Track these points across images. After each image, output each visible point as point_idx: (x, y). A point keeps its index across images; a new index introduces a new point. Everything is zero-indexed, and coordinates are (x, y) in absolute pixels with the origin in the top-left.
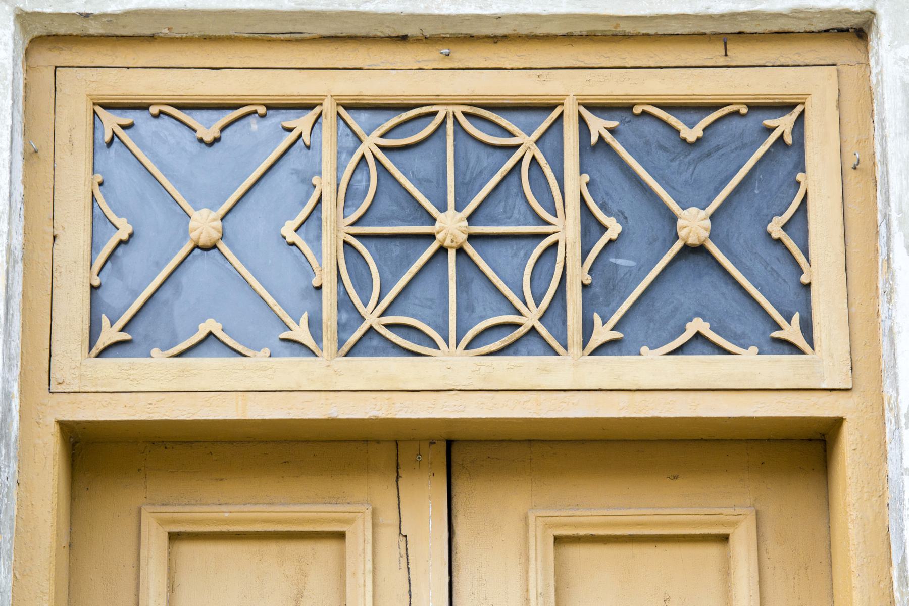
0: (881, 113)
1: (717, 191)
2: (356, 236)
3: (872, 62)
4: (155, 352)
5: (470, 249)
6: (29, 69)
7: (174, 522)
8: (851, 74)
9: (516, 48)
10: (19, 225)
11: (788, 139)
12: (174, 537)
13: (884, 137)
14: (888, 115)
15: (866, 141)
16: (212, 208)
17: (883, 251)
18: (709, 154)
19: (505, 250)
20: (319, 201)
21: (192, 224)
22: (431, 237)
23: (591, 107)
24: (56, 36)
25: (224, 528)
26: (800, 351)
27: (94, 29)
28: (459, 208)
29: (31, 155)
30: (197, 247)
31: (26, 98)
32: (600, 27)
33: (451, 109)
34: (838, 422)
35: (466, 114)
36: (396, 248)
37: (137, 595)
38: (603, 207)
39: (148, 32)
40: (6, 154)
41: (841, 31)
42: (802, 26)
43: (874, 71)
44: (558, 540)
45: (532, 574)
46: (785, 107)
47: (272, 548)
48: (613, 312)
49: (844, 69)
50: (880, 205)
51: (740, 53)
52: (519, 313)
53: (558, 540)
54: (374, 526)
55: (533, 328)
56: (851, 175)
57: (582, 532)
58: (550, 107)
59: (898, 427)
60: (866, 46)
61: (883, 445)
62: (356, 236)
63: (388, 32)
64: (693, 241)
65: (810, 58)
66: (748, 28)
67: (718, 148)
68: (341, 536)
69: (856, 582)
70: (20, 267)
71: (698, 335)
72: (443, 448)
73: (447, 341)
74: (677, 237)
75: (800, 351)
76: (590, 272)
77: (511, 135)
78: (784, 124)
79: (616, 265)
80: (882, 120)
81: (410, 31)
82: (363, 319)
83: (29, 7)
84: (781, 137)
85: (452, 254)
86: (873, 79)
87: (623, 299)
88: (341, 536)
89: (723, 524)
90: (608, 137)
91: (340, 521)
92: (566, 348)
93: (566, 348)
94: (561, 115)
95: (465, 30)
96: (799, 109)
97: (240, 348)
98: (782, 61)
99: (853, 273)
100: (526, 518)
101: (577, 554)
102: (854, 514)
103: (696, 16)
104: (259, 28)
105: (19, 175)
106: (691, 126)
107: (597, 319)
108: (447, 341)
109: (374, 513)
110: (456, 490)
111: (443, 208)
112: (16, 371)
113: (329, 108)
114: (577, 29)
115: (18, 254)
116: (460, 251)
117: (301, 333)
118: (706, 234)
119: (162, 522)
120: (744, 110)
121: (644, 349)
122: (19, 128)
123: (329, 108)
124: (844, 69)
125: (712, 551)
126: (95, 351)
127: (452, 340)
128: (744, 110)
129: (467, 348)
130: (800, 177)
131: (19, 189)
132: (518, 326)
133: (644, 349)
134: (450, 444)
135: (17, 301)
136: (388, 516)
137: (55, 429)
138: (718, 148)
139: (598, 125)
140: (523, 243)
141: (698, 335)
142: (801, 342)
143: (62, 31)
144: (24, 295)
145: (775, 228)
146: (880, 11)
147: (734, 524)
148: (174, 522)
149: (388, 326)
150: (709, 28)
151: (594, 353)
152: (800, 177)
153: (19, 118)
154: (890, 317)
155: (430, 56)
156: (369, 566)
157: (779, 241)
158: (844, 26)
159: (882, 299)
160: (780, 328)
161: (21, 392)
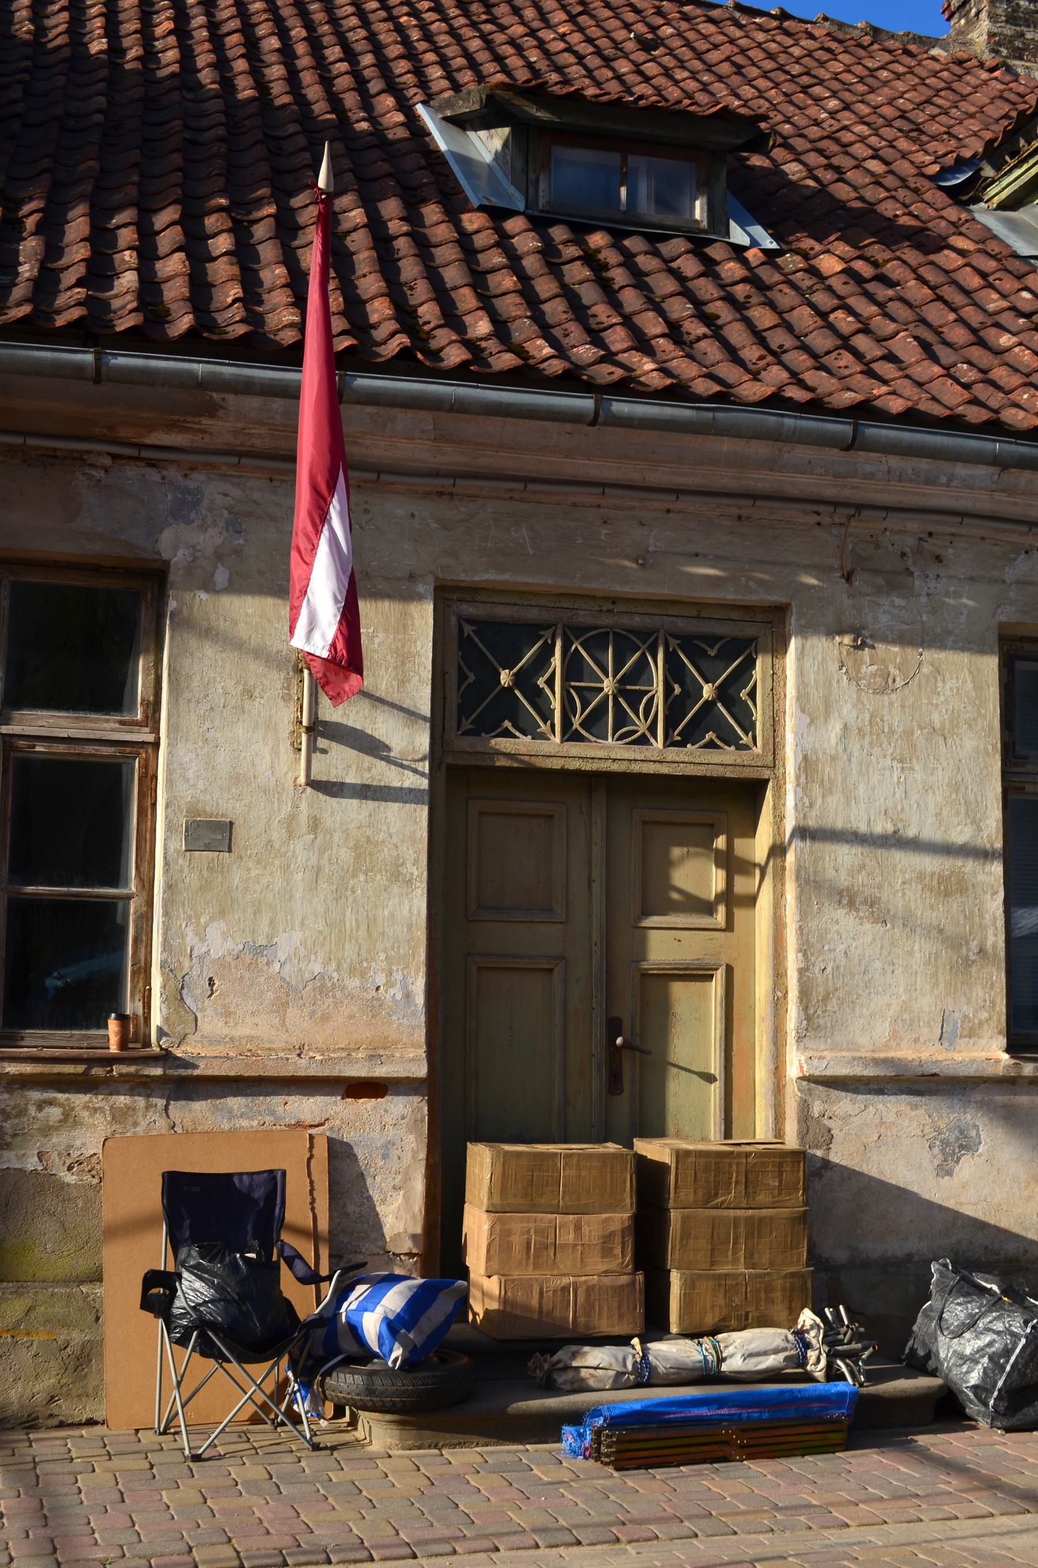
58: (651, 634)
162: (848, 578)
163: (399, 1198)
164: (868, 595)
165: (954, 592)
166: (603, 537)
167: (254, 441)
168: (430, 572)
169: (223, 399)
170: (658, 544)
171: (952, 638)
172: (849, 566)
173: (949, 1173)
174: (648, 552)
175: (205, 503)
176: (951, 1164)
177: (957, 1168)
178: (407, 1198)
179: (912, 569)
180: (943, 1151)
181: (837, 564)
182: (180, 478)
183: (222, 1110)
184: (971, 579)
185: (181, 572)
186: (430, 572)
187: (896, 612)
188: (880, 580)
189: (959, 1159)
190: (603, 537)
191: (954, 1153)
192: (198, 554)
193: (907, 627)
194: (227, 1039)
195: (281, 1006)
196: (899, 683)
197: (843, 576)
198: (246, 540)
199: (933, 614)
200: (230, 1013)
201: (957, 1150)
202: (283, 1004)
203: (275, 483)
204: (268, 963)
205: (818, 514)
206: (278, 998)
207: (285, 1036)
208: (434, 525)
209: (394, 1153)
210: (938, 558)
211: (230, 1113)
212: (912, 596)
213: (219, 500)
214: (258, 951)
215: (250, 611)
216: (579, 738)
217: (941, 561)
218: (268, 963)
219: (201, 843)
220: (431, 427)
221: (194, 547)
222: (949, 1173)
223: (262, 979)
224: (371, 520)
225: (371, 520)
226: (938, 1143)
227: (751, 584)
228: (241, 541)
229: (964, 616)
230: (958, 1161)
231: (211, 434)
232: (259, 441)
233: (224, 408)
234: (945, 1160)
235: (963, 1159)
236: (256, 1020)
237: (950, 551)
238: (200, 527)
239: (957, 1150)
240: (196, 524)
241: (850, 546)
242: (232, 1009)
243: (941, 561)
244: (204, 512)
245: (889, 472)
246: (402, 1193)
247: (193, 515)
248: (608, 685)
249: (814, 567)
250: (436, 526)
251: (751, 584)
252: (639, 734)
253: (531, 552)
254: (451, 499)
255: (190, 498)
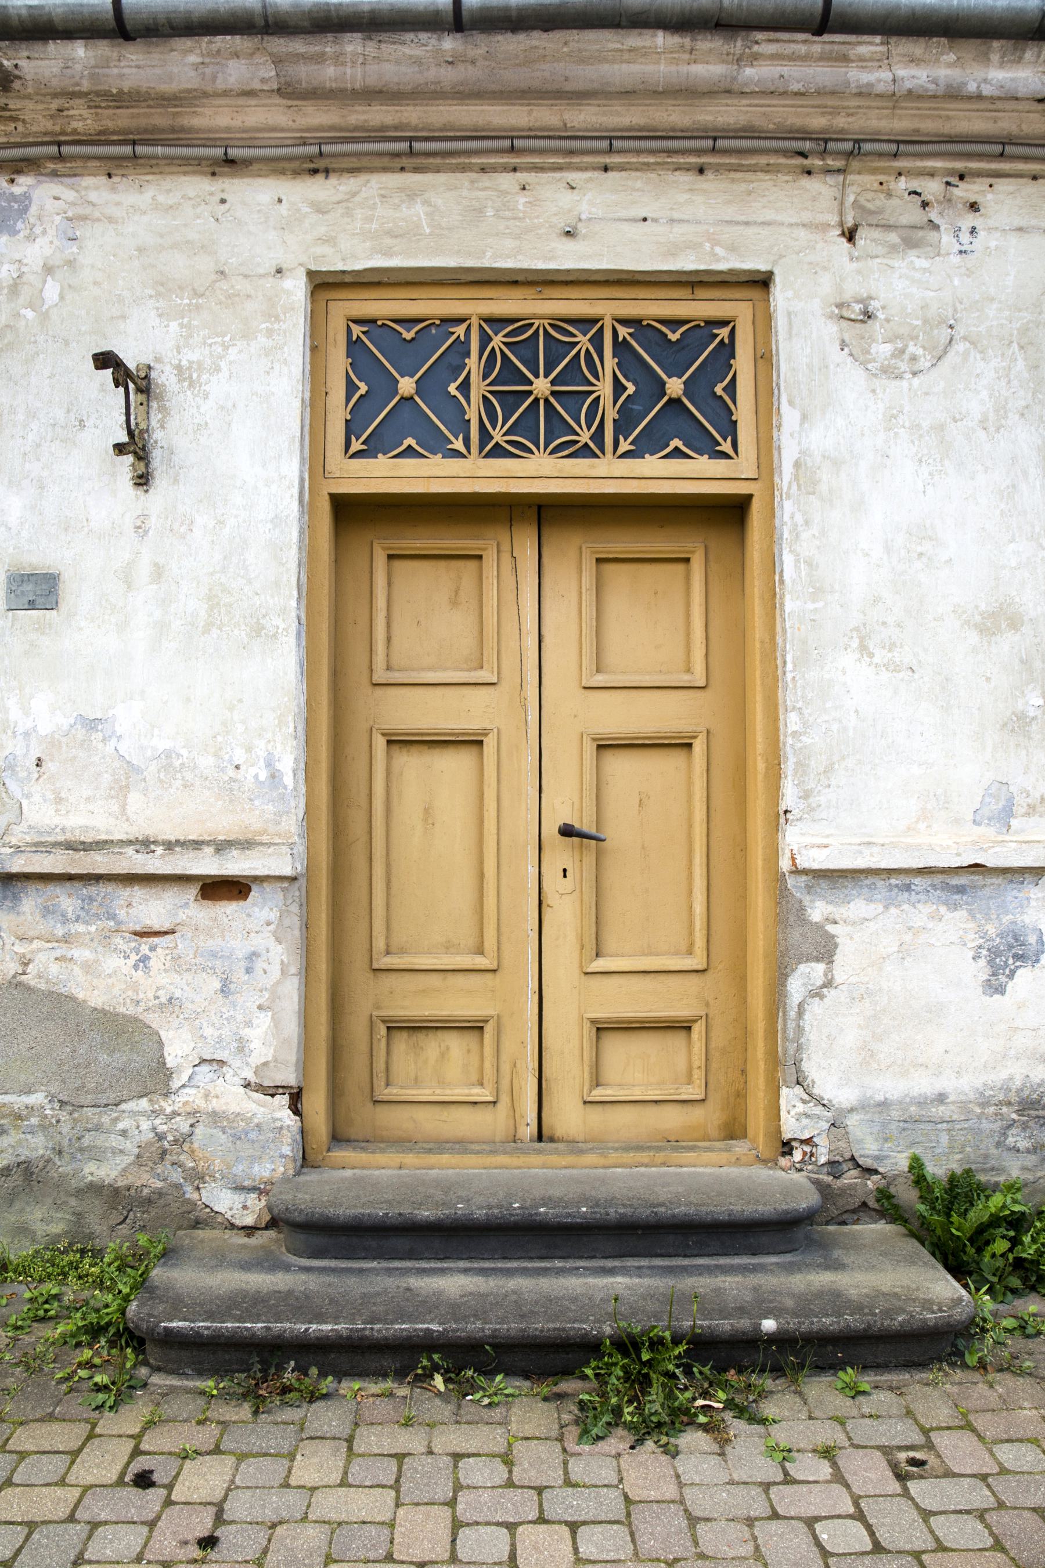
0: (776, 328)
1: (688, 369)
2: (490, 392)
3: (771, 300)
4: (380, 455)
5: (552, 400)
6: (313, 302)
7: (390, 549)
8: (760, 305)
9: (154, 890)
10: (308, 387)
11: (726, 341)
12: (391, 557)
13: (777, 341)
14: (780, 329)
15: (768, 343)
16: (412, 376)
17: (776, 403)
18: (683, 348)
19: (570, 401)
20: (469, 372)
21: (400, 386)
22: (530, 393)
23: (620, 321)
24: (328, 284)
25: (417, 552)
26: (731, 458)
27: (348, 279)
28: (546, 376)
29: (314, 349)
30: (402, 398)
31: (311, 317)
32: (624, 276)
33: (542, 321)
34: (749, 497)
35: (550, 324)
36: (511, 399)
37: (371, 587)
38: (625, 376)
39: (376, 280)
40: (301, 348)
41: (755, 282)
42: (734, 279)
43: (772, 305)
44: (598, 560)
45: (584, 579)
46: (724, 323)
47: (442, 564)
48: (630, 435)
49: (756, 303)
50: (774, 378)
51: (700, 293)
52: (578, 435)
53: (598, 560)
54: (498, 552)
55: (586, 444)
56: (760, 361)
57: (611, 556)
58: (596, 321)
59: (782, 500)
60: (768, 293)
61: (773, 509)
62: (490, 392)
63: (508, 279)
64: (674, 396)
65: (738, 296)
66: (705, 279)
67: (688, 345)
68: (480, 557)
69: (756, 583)
70: (308, 409)
71: (676, 448)
72: (535, 509)
73: (539, 450)
74: (665, 394)
75: (731, 458)
76: (618, 412)
77: (575, 336)
78: (724, 333)
79: (632, 409)
80: (777, 332)
81: (520, 278)
82: (492, 438)
83: (313, 268)
84: (722, 340)
85: (542, 402)
86: (772, 309)
87: (635, 428)
88: (480, 557)
89: (687, 552)
90: (628, 338)
91: (479, 549)
92: (604, 454)
93: (604, 454)
94: (602, 326)
95: (550, 278)
96: (732, 324)
97: (426, 453)
98: (723, 297)
99: (760, 415)
100: (581, 548)
101: (610, 568)
102: (757, 546)
103: (677, 272)
104: (437, 277)
105: (308, 360)
106: (674, 332)
107: (621, 438)
108: (539, 450)
109: (498, 545)
110: (543, 532)
111: (537, 376)
112: (307, 466)
113: (475, 322)
114: (612, 278)
115: (308, 402)
116: (546, 400)
117: (459, 445)
118: (681, 392)
119: (384, 549)
120: (702, 324)
121: (647, 456)
122: (308, 334)
123: (475, 322)
124: (756, 303)
125: (680, 567)
126: (348, 455)
127: (542, 450)
128: (702, 324)
129: (550, 454)
130: (732, 362)
131: (308, 367)
132: (577, 442)
133: (647, 456)
134: (540, 507)
135: (307, 428)
136: (506, 547)
137: (327, 497)
138: (688, 345)
139: (623, 332)
140: (581, 396)
141: (676, 448)
142: (731, 453)
143: (331, 281)
144: (311, 425)
145: (719, 390)
146: (776, 272)
147: (693, 552)
148: (390, 549)
149: (507, 442)
150: (684, 278)
151: (620, 457)
152: (732, 362)
153: (308, 328)
154: (779, 439)
155: (529, 292)
156: (495, 573)
157: (721, 397)
158: (756, 279)
159: (775, 430)
160: (720, 445)
161: (310, 478)
162: (850, 236)
163: (264, 1020)
164: (877, 257)
165: (997, 248)
166: (521, 207)
167: (75, 124)
168: (301, 265)
169: (16, 66)
170: (594, 210)
171: (995, 306)
172: (850, 222)
173: (1001, 990)
174: (580, 220)
175: (33, 210)
176: (1003, 979)
177: (1010, 984)
178: (276, 1021)
179: (936, 221)
180: (991, 962)
181: (834, 219)
182: (5, 184)
183: (53, 913)
184: (1020, 229)
185: (5, 291)
186: (301, 265)
187: (917, 275)
188: (893, 237)
189: (1013, 973)
190: (521, 207)
191: (1006, 965)
192: (24, 269)
193: (932, 294)
194: (58, 830)
195: (121, 790)
196: (924, 363)
197: (843, 234)
198: (80, 248)
199: (968, 276)
200: (61, 799)
201: (1011, 961)
202: (121, 788)
203: (115, 179)
204: (104, 740)
205: (803, 154)
206: (116, 781)
207: (125, 825)
208: (306, 209)
209: (259, 965)
210: (974, 207)
211: (63, 916)
212: (938, 255)
213: (50, 205)
214: (92, 724)
215: (83, 329)
216: (498, 452)
217: (977, 210)
218: (104, 740)
219: (26, 601)
220: (273, 73)
221: (20, 261)
222: (1001, 990)
223: (96, 759)
224: (229, 210)
225: (229, 210)
226: (984, 952)
227: (718, 250)
228: (75, 250)
229: (1012, 278)
230: (1012, 975)
231: (24, 121)
232: (81, 124)
233: (19, 77)
234: (994, 975)
235: (1019, 972)
236: (91, 807)
237: (990, 196)
238: (27, 237)
239: (1011, 961)
240: (22, 234)
241: (851, 198)
242: (63, 795)
243: (977, 210)
244: (32, 220)
245: (894, 80)
246: (270, 1014)
247: (20, 225)
248: (541, 386)
249: (804, 225)
250: (309, 210)
251: (718, 250)
252: (580, 444)
253: (428, 231)
254: (327, 177)
255: (16, 206)
